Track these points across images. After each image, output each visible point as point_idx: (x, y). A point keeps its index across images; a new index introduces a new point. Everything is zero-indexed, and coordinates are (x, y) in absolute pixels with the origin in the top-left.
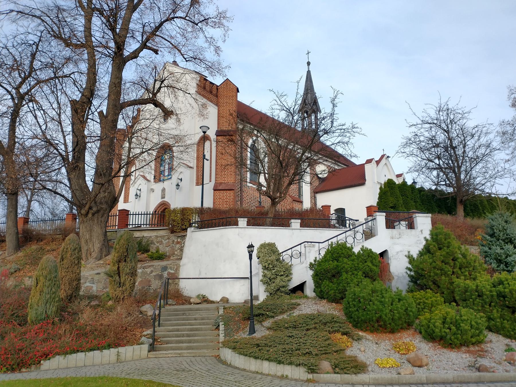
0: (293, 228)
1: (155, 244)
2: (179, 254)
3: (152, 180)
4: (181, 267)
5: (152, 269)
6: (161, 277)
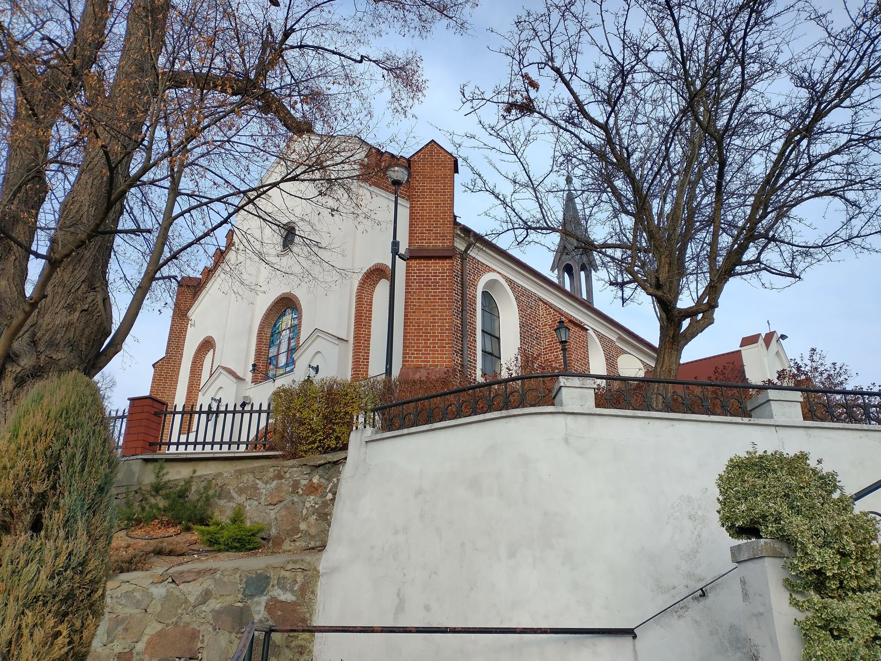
0: (778, 419)
1: (231, 499)
2: (313, 531)
3: (249, 376)
4: (322, 580)
5: (207, 583)
6: (239, 618)
